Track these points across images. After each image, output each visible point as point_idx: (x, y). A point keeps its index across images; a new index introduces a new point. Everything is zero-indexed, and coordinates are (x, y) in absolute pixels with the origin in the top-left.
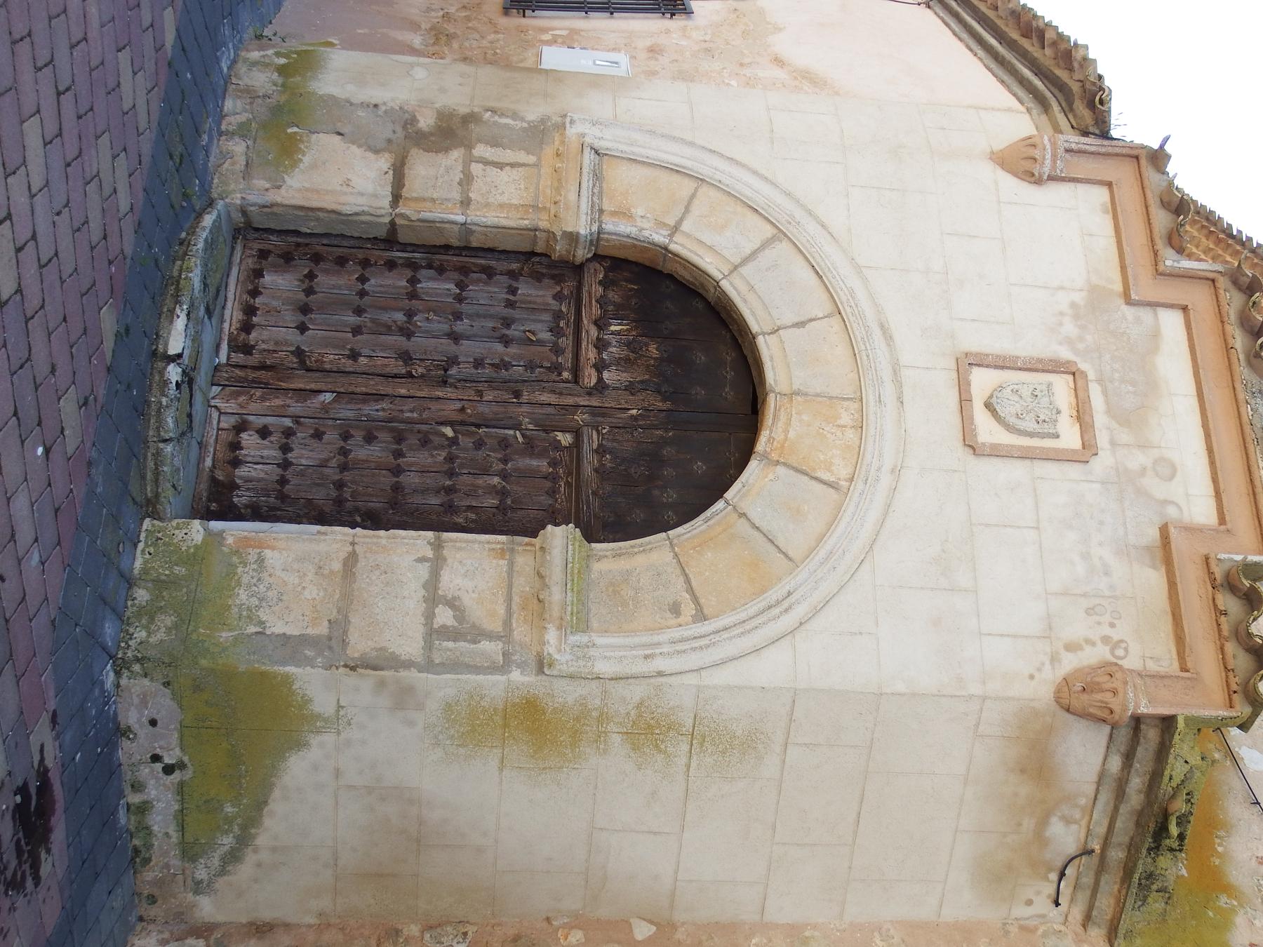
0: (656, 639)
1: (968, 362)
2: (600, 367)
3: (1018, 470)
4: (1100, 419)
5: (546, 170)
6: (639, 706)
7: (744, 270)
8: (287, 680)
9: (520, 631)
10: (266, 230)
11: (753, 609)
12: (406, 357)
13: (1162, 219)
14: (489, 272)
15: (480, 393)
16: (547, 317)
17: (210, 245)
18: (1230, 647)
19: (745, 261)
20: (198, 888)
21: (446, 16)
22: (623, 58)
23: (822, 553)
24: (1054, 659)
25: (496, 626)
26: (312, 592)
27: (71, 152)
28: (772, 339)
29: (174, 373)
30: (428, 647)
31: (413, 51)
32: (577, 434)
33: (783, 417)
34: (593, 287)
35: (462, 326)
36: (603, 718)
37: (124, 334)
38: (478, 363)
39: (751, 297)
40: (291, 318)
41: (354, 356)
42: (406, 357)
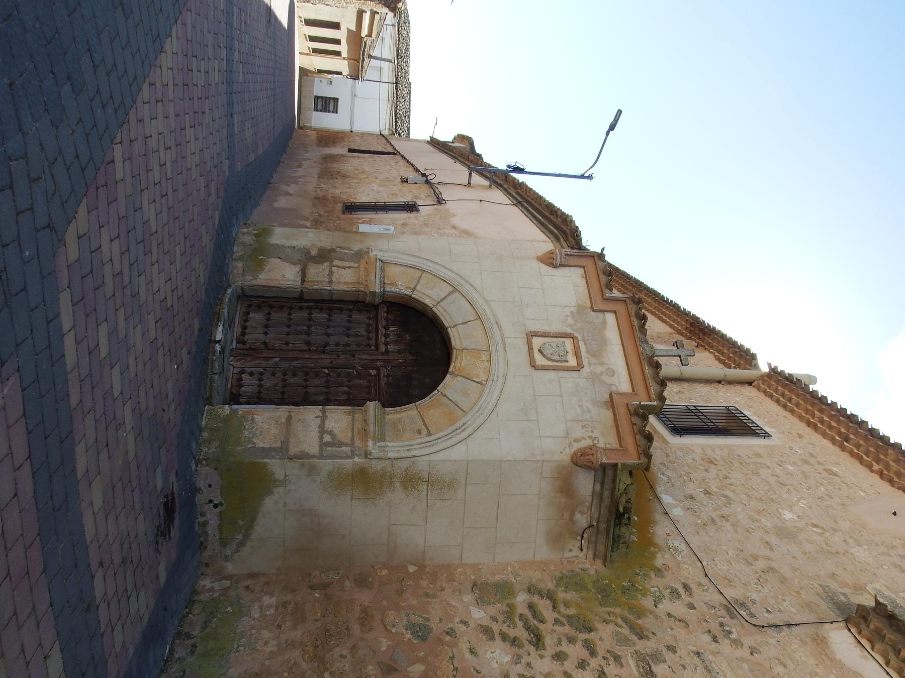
0: (412, 443)
1: (531, 335)
2: (386, 344)
3: (552, 375)
4: (584, 355)
5: (362, 269)
6: (405, 471)
7: (441, 304)
8: (265, 465)
9: (358, 443)
10: (252, 296)
11: (450, 430)
12: (308, 343)
13: (604, 279)
14: (341, 310)
15: (339, 356)
16: (364, 326)
17: (230, 301)
18: (638, 437)
19: (441, 300)
20: (227, 559)
21: (320, 215)
22: (392, 228)
23: (476, 408)
24: (570, 445)
25: (348, 441)
26: (274, 431)
27: (188, 259)
28: (453, 329)
29: (218, 347)
30: (321, 449)
31: (307, 228)
32: (378, 370)
33: (459, 358)
34: (382, 314)
35: (330, 331)
36: (392, 476)
37: (201, 330)
38: (337, 345)
39: (445, 314)
40: (261, 330)
41: (287, 343)
42: (308, 343)
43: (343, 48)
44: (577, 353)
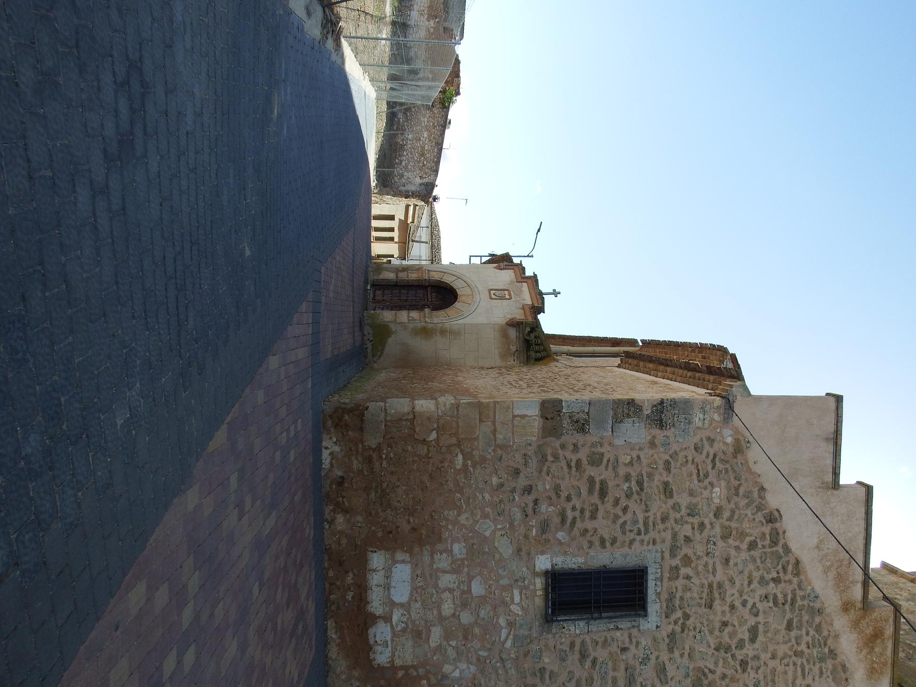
20: (375, 362)
34: (429, 289)
43: (396, 235)
44: (510, 295)
